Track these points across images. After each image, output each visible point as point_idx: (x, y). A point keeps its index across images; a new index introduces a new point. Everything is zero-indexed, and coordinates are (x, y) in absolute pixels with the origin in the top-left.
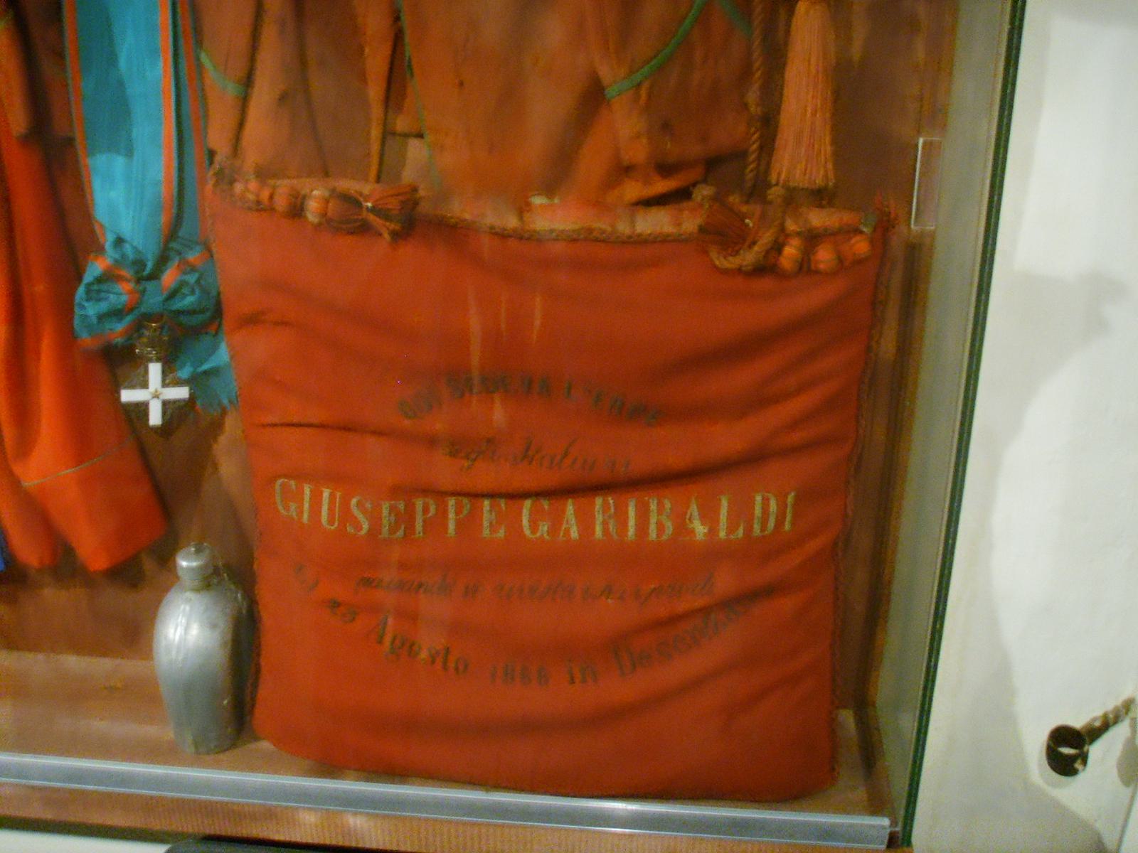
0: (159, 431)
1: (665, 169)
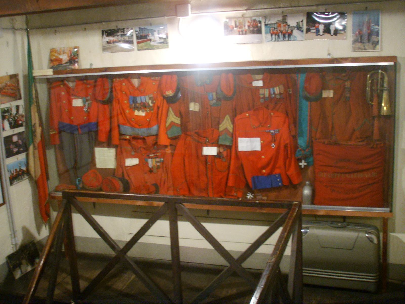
1: (361, 138)
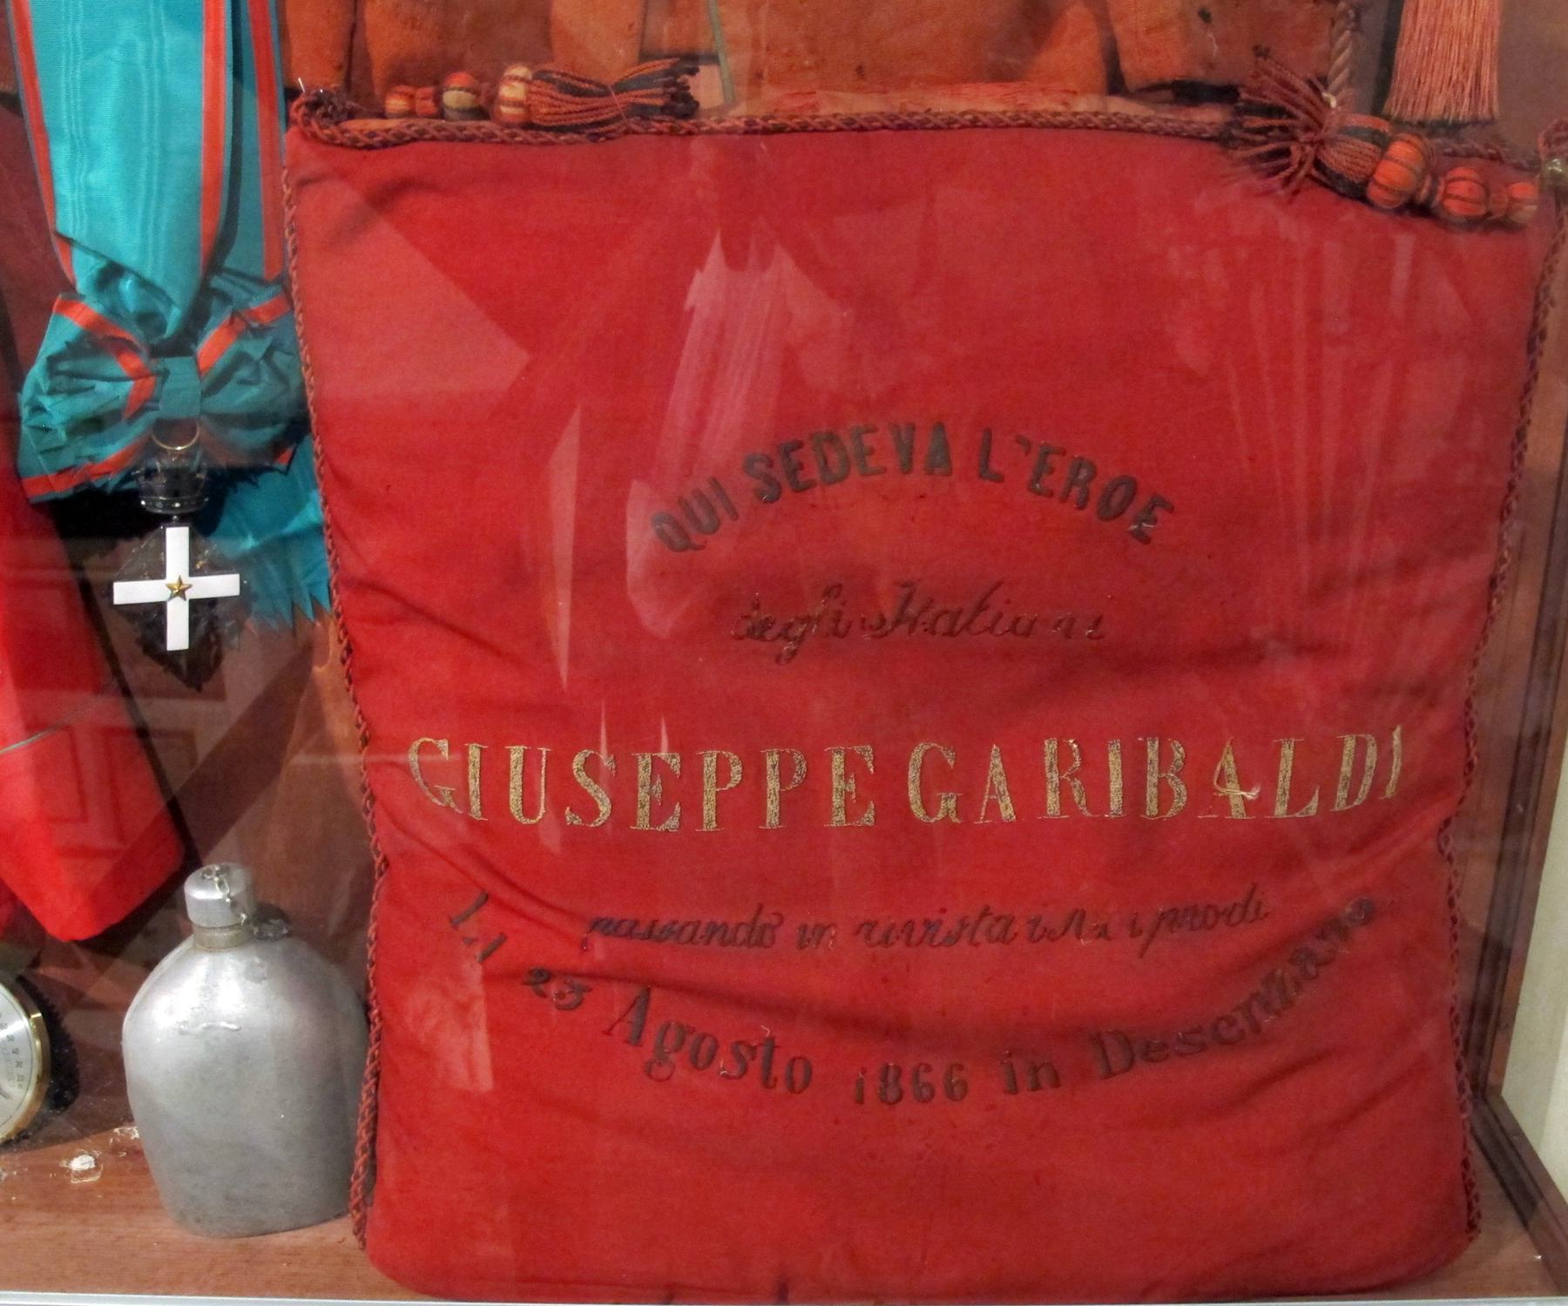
0: (183, 662)
